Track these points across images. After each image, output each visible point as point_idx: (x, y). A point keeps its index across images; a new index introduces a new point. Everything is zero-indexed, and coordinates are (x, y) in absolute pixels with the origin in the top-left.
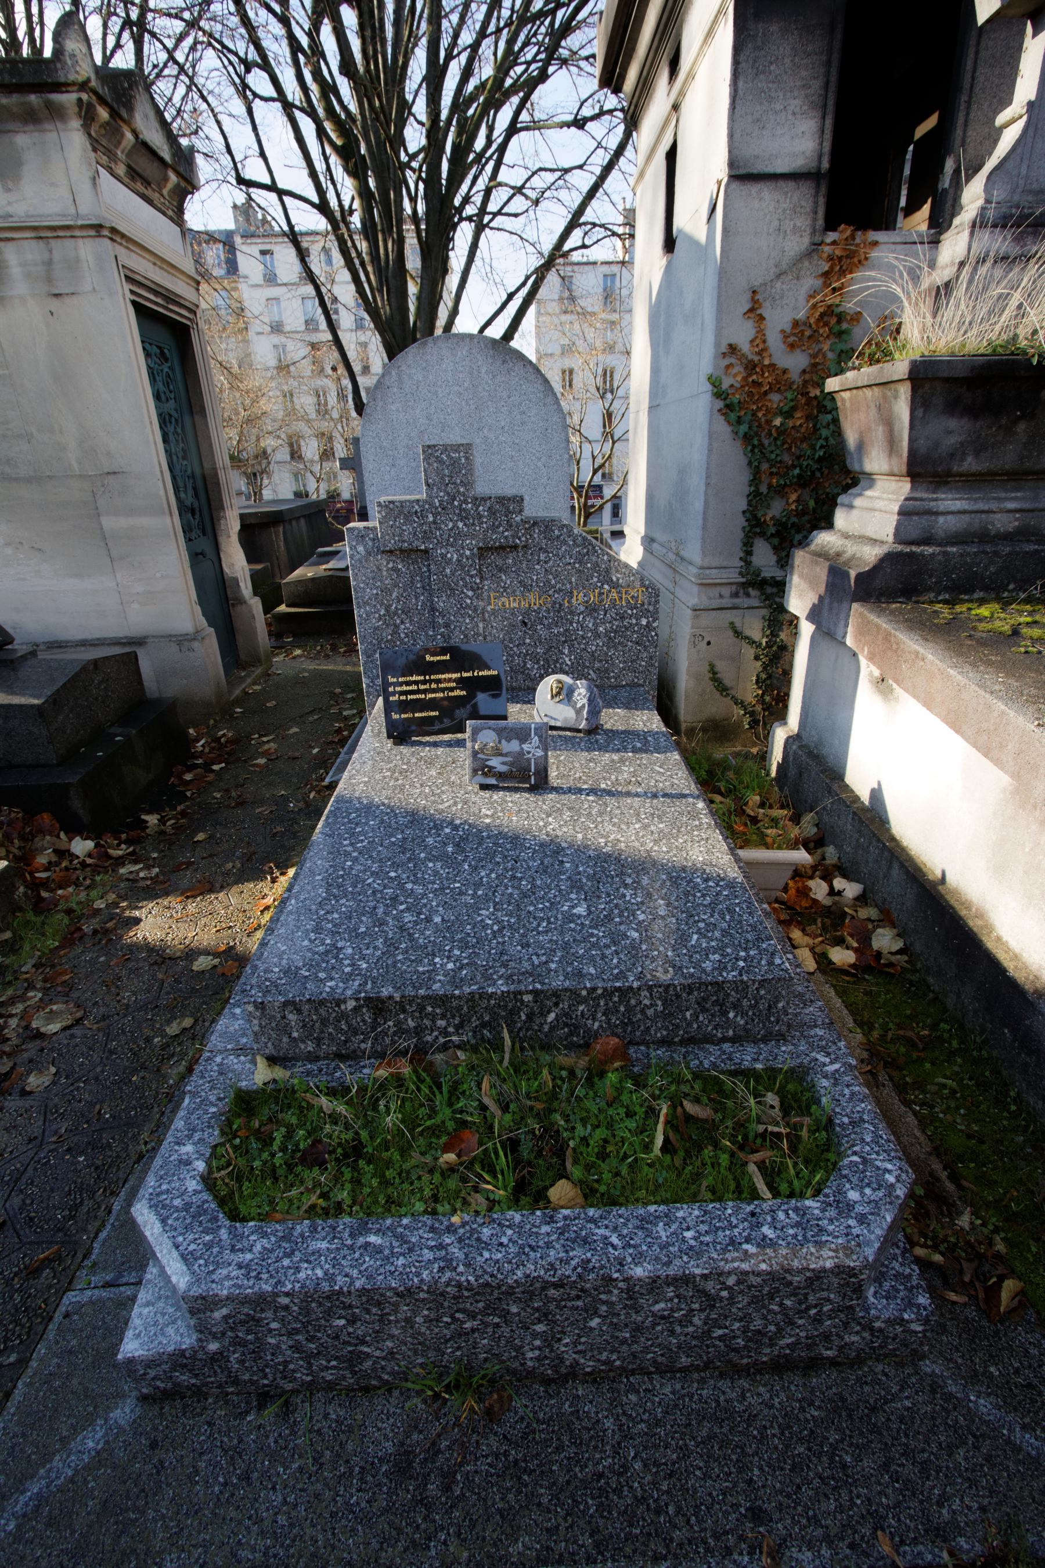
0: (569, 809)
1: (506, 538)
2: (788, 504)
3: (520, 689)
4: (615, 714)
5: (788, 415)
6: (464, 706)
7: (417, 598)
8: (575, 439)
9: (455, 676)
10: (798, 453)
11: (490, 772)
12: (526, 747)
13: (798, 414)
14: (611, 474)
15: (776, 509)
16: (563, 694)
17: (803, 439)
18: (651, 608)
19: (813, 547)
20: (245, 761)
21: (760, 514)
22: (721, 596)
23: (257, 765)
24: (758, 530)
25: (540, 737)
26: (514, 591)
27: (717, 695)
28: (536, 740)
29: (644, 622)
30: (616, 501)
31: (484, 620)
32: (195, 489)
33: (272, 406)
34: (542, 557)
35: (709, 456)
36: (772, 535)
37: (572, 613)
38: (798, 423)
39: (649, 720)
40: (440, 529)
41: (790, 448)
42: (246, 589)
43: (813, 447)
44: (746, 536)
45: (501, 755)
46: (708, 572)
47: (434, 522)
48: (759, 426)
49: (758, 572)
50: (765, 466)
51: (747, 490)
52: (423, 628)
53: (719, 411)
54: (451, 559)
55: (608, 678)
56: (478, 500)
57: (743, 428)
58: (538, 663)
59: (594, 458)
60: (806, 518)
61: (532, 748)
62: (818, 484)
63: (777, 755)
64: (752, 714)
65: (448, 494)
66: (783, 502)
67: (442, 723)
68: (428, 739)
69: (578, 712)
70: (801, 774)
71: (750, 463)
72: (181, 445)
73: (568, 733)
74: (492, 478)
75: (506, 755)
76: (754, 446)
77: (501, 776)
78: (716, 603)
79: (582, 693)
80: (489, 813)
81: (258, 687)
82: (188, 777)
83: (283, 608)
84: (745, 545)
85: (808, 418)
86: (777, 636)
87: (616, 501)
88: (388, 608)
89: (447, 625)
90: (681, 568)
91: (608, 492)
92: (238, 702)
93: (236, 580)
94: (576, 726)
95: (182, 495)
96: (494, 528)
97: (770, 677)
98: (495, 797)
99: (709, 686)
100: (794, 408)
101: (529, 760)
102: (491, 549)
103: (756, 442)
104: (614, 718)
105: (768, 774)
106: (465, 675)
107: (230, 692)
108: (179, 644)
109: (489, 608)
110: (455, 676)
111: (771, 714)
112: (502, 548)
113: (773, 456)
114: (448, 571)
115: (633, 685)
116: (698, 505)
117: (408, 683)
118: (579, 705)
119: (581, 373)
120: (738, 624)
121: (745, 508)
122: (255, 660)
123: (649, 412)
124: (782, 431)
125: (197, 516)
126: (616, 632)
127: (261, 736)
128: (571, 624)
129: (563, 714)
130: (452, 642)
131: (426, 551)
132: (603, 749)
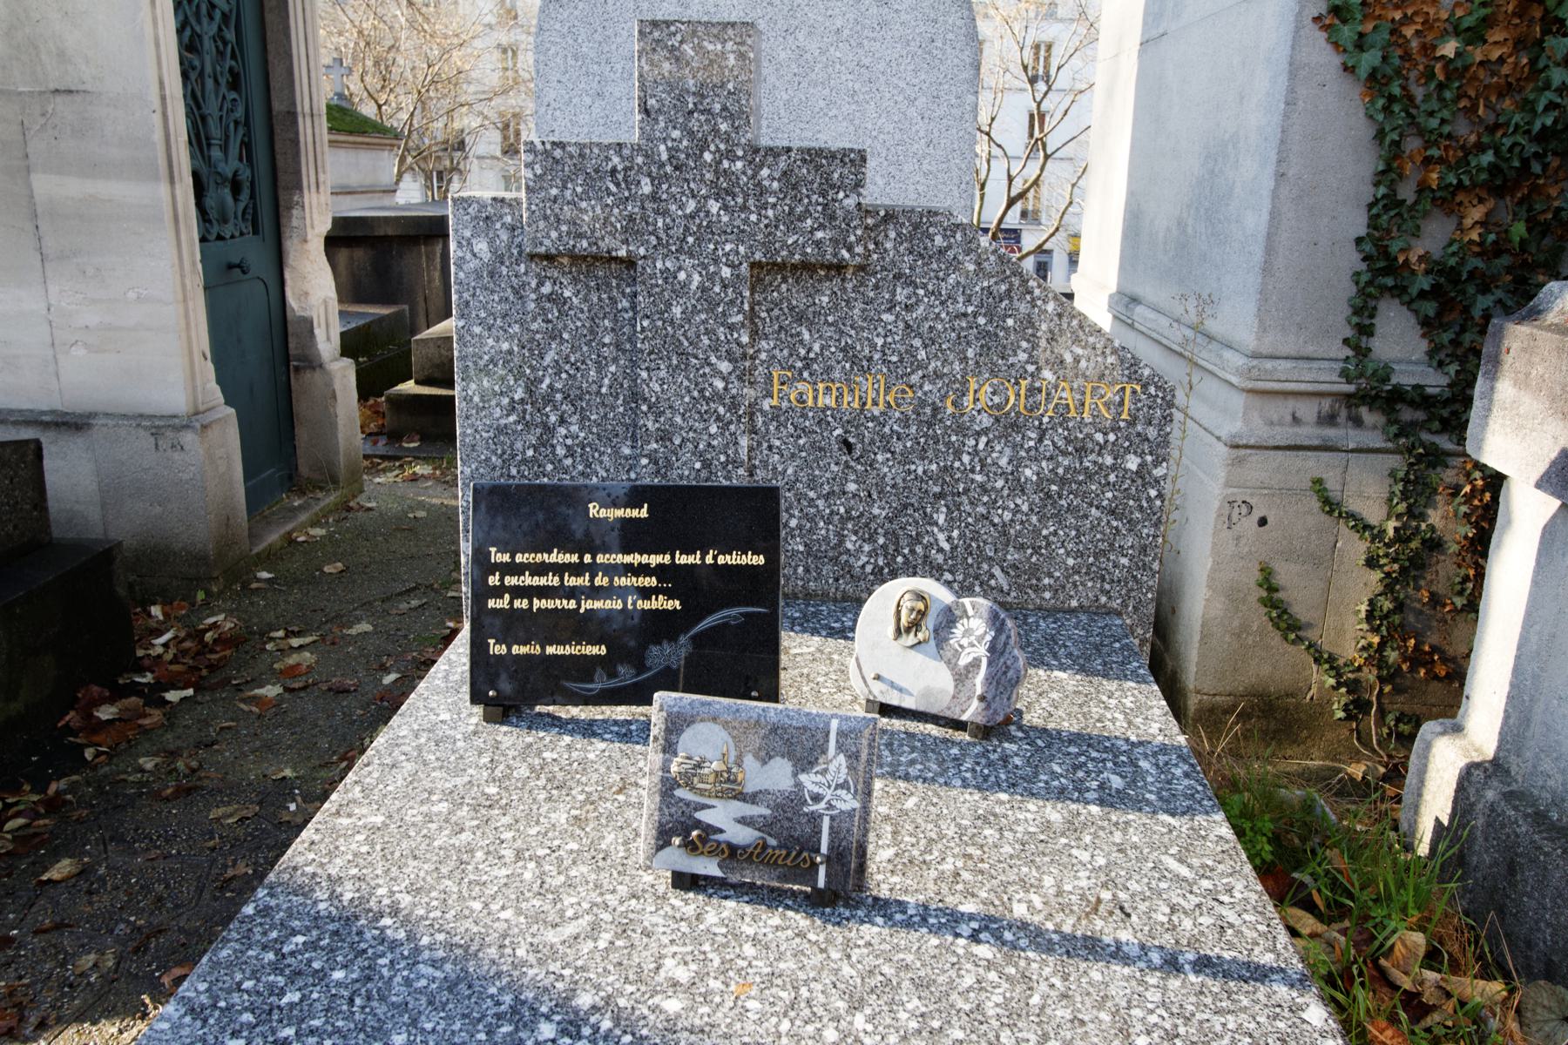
0: (921, 985)
1: (818, 243)
2: (1460, 227)
3: (825, 597)
4: (1055, 685)
5: (1474, 35)
6: (673, 638)
7: (600, 368)
8: (982, 148)
9: (655, 560)
10: (1491, 119)
11: (700, 839)
12: (809, 781)
13: (1496, 35)
14: (1036, 212)
15: (1432, 238)
16: (926, 628)
17: (1506, 89)
18: (1152, 433)
19: (1551, 317)
20: (238, 688)
21: (1394, 247)
22: (1296, 420)
23: (256, 700)
24: (1389, 281)
25: (853, 757)
26: (828, 370)
27: (1275, 638)
28: (837, 764)
29: (1132, 463)
30: (1043, 258)
31: (753, 431)
32: (247, 145)
33: (486, 70)
34: (901, 294)
35: (1286, 116)
36: (1423, 295)
37: (961, 430)
38: (1495, 54)
39: (1139, 708)
40: (665, 213)
41: (1475, 107)
42: (327, 342)
43: (1528, 106)
44: (1362, 292)
45: (741, 797)
46: (1269, 365)
47: (654, 197)
48: (1407, 56)
49: (1384, 374)
50: (1413, 144)
51: (1368, 192)
52: (608, 437)
53: (1316, 19)
54: (685, 285)
55: (1037, 589)
56: (758, 155)
57: (1370, 59)
58: (871, 539)
59: (1010, 179)
60: (1505, 260)
61: (827, 786)
62: (1535, 189)
63: (1435, 802)
64: (1354, 686)
65: (691, 134)
66: (1450, 225)
67: (613, 674)
68: (575, 711)
69: (962, 677)
70: (1512, 869)
71: (1380, 135)
72: (229, 63)
73: (932, 729)
74: (795, 110)
75: (753, 799)
76: (1391, 99)
77: (732, 854)
78: (1284, 435)
79: (974, 630)
80: (683, 975)
81: (318, 532)
82: (105, 713)
83: (409, 387)
84: (1357, 311)
85: (1519, 44)
86: (1422, 517)
87: (1043, 258)
88: (531, 385)
89: (664, 437)
90: (1205, 356)
91: (1029, 241)
92: (268, 558)
93: (308, 324)
94: (954, 714)
95: (216, 153)
96: (792, 220)
97: (1400, 607)
98: (711, 918)
99: (1259, 618)
100: (1488, 22)
101: (815, 819)
102: (781, 267)
103: (1397, 91)
104: (1053, 697)
105: (1409, 848)
106: (683, 559)
107: (253, 536)
108: (156, 433)
109: (766, 405)
110: (655, 560)
111: (1397, 690)
112: (807, 267)
113: (1434, 123)
114: (677, 311)
115: (1095, 611)
116: (1255, 221)
117: (540, 569)
118: (964, 660)
119: (997, 43)
120: (1332, 485)
121: (1363, 232)
122: (327, 478)
123: (1141, 53)
124: (1456, 70)
125: (245, 196)
126: (1063, 482)
127: (290, 634)
128: (958, 455)
129: (923, 679)
130: (673, 474)
131: (630, 263)
132: (1022, 784)
